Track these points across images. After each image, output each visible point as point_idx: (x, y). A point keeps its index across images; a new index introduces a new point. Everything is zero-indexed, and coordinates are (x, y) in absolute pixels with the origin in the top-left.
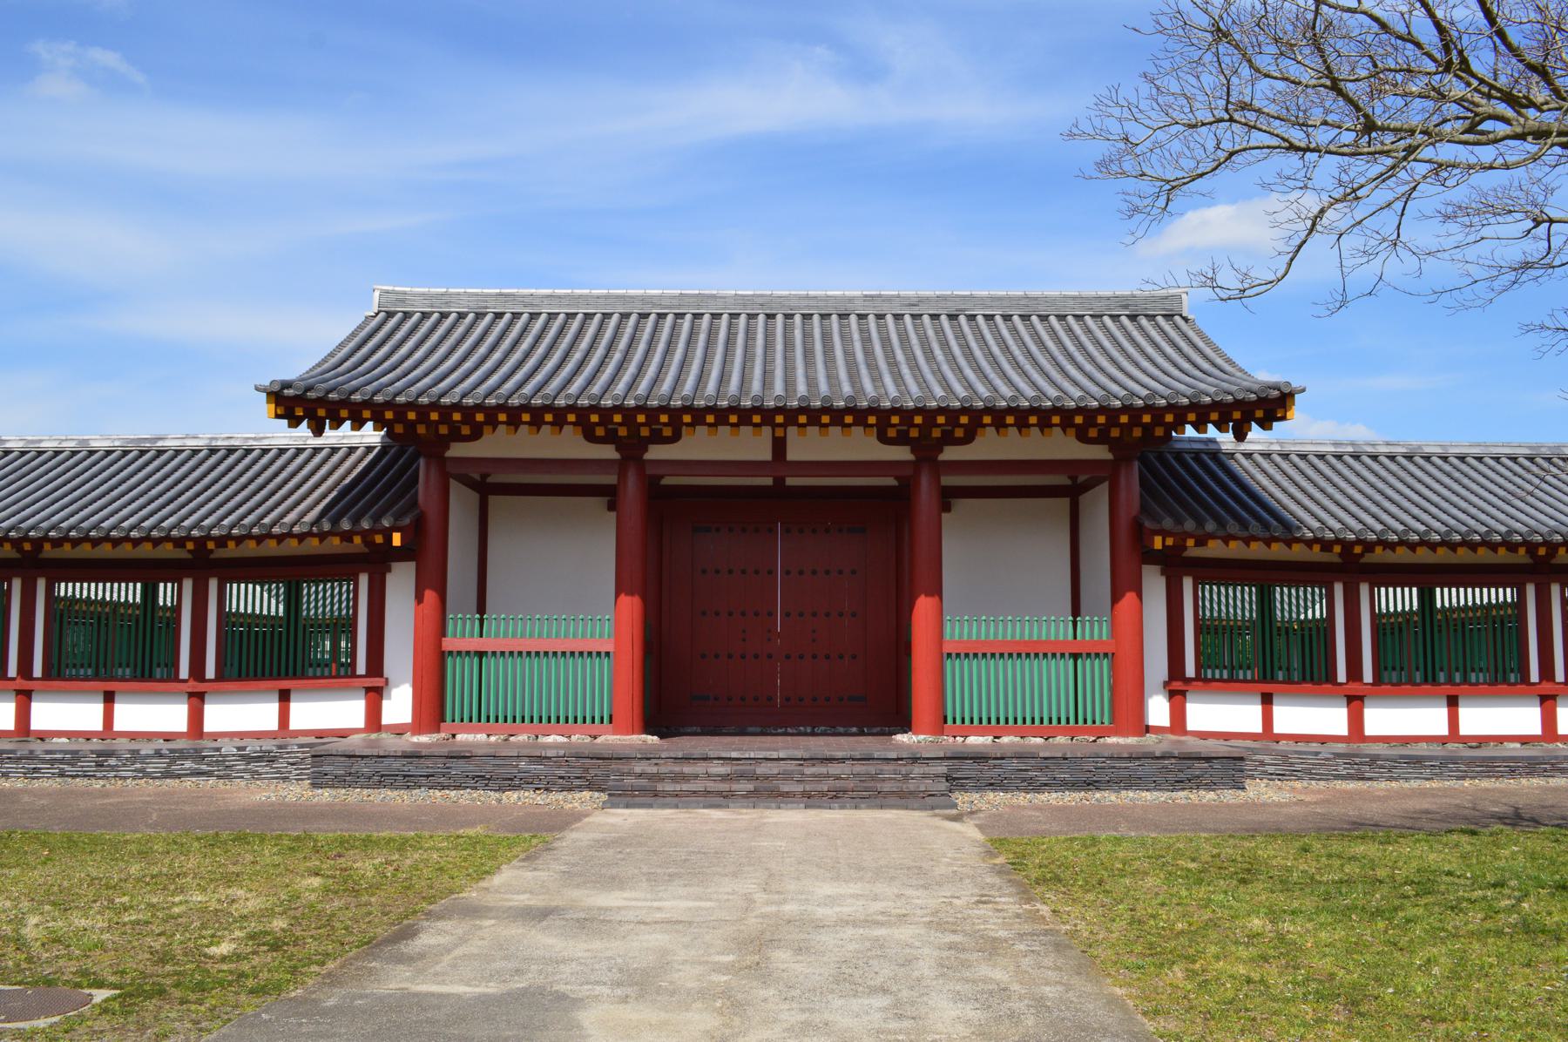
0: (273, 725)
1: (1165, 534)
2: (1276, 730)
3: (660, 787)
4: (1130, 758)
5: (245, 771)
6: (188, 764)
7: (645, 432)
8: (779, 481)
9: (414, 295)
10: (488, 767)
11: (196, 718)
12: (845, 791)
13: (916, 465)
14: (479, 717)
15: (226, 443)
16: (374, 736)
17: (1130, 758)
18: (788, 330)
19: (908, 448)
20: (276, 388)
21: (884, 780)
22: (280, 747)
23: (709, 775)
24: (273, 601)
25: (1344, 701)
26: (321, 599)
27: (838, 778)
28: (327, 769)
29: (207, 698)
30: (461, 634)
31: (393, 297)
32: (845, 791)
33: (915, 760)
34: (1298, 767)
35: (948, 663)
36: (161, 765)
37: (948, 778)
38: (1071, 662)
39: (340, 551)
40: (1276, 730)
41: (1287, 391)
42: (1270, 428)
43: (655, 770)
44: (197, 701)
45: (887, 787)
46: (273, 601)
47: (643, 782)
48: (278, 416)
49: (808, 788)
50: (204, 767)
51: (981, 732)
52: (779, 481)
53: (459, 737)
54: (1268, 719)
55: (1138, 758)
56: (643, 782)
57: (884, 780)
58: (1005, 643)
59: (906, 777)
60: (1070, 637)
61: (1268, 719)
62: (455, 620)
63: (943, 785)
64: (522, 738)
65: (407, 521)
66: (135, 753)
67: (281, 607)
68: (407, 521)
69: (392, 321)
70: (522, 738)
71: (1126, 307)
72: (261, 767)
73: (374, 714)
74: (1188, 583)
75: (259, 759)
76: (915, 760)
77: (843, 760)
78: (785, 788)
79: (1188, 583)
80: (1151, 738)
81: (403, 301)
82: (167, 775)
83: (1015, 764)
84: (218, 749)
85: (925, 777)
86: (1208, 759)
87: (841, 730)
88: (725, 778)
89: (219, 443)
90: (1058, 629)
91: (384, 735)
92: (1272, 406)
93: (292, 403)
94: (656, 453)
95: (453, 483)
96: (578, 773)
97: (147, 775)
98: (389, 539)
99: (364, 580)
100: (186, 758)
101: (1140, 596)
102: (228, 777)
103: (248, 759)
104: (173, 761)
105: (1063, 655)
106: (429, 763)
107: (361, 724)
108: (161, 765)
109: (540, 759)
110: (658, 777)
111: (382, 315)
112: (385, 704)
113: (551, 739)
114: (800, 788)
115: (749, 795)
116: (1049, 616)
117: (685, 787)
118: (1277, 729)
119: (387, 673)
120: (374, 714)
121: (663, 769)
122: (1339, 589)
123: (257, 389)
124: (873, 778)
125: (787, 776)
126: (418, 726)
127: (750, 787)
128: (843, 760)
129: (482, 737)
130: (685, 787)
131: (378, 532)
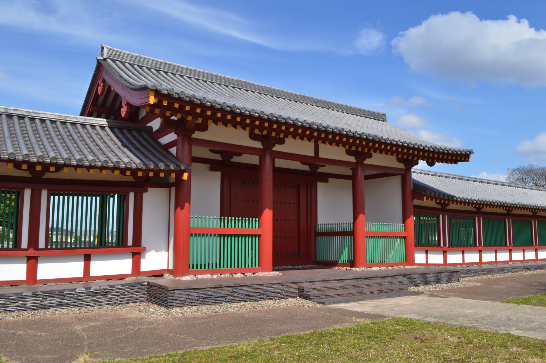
0: (81, 274)
5: (90, 301)
6: (55, 300)
9: (124, 54)
10: (250, 291)
11: (32, 272)
13: (357, 164)
19: (354, 157)
22: (111, 286)
25: (131, 255)
28: (176, 297)
29: (39, 259)
31: (114, 53)
35: (191, 238)
36: (36, 301)
38: (219, 238)
39: (119, 180)
44: (32, 263)
50: (65, 301)
54: (445, 259)
58: (209, 229)
60: (219, 227)
61: (445, 259)
62: (194, 218)
66: (19, 296)
72: (101, 299)
74: (44, 193)
75: (99, 294)
79: (44, 193)
80: (415, 267)
81: (119, 55)
82: (41, 307)
84: (74, 290)
86: (453, 272)
87: (297, 267)
90: (399, 228)
96: (285, 290)
97: (26, 308)
100: (53, 296)
101: (190, 204)
102: (80, 305)
103: (93, 294)
104: (45, 298)
105: (215, 235)
106: (225, 290)
107: (129, 272)
108: (36, 301)
112: (142, 261)
115: (356, 294)
116: (198, 216)
118: (448, 262)
119: (143, 244)
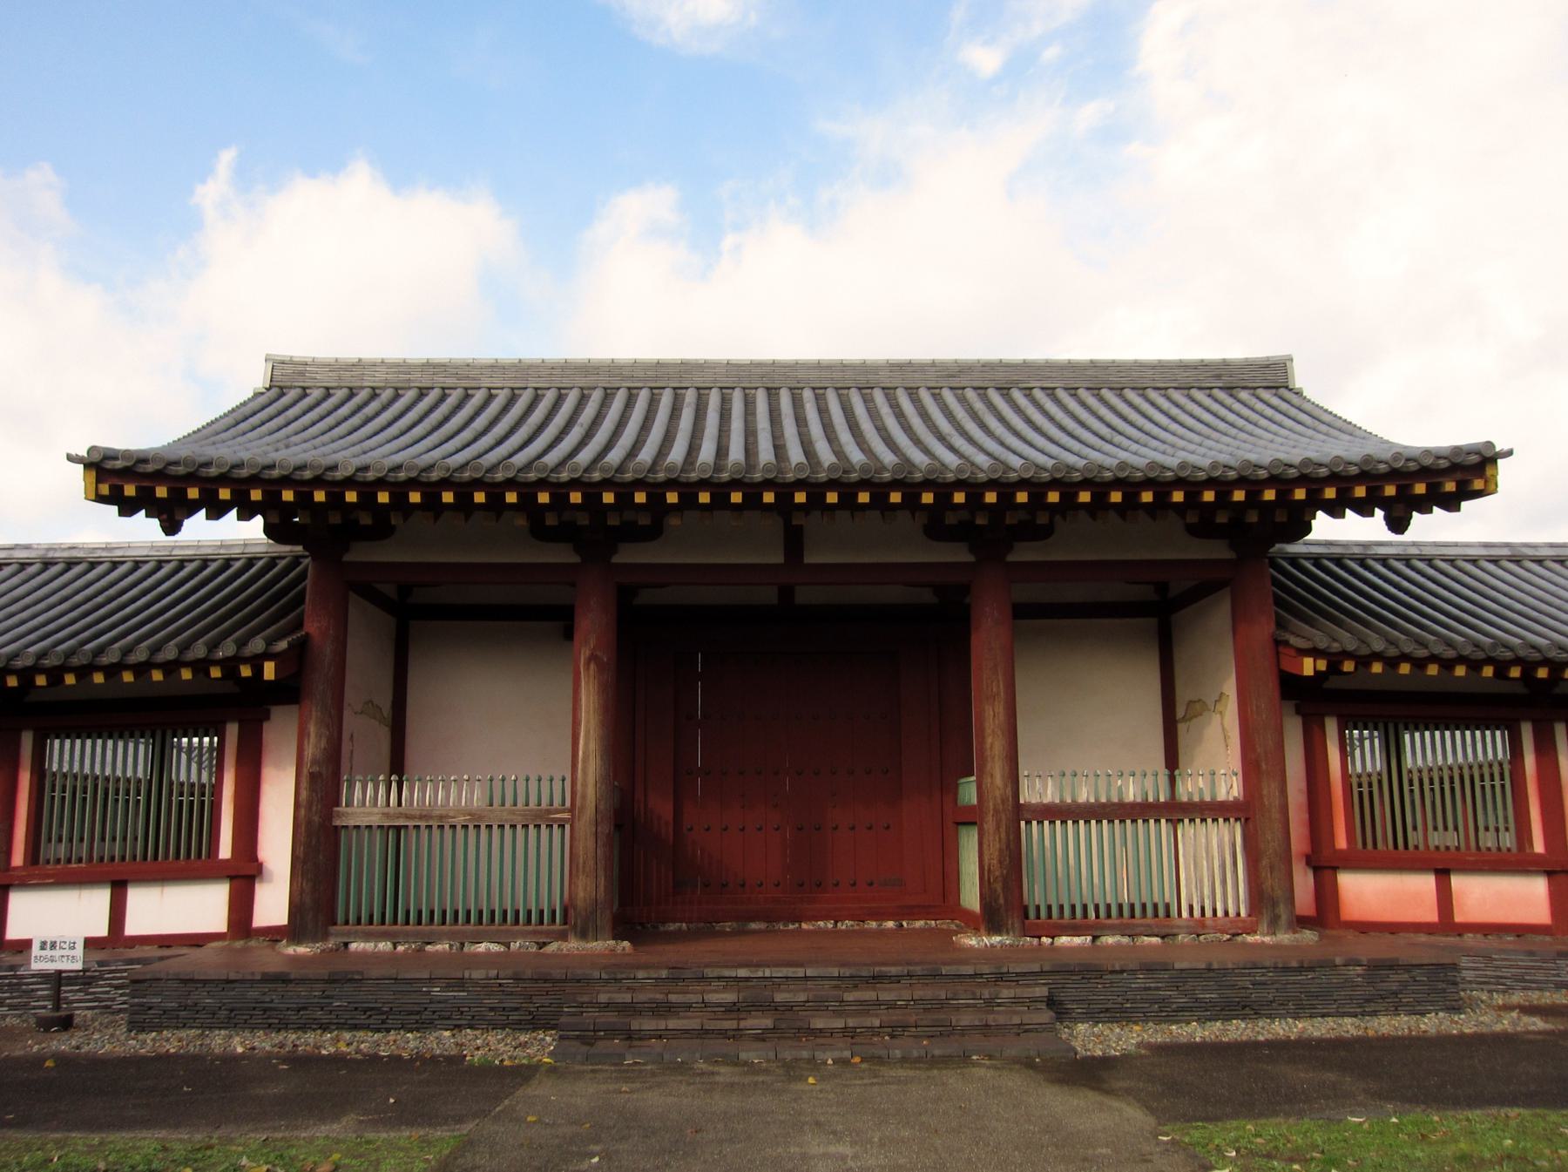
1: (1315, 653)
2: (1458, 919)
3: (635, 1025)
4: (1301, 969)
7: (613, 521)
8: (786, 592)
12: (905, 1027)
14: (372, 924)
15: (66, 554)
16: (239, 944)
17: (1301, 969)
18: (797, 403)
20: (96, 457)
21: (958, 1008)
23: (705, 1004)
24: (194, 766)
26: (191, 757)
27: (892, 1006)
30: (366, 802)
32: (905, 1027)
33: (1000, 978)
34: (1506, 972)
37: (1051, 1002)
40: (1458, 919)
41: (1488, 454)
42: (1458, 509)
43: (627, 998)
45: (966, 1019)
46: (194, 766)
47: (611, 1018)
48: (100, 499)
49: (851, 1022)
51: (1075, 931)
52: (786, 592)
53: (353, 946)
55: (1311, 969)
56: (611, 1018)
57: (958, 1008)
59: (990, 1003)
63: (1046, 1016)
64: (442, 947)
65: (283, 645)
67: (205, 775)
68: (283, 645)
69: (291, 391)
70: (442, 947)
71: (1218, 377)
73: (241, 906)
74: (1331, 726)
76: (1000, 978)
77: (897, 979)
78: (818, 1023)
81: (302, 374)
83: (1141, 980)
85: (1017, 1001)
88: (732, 1009)
89: (57, 555)
91: (253, 943)
92: (1462, 475)
93: (120, 479)
94: (629, 555)
95: (353, 596)
98: (258, 671)
99: (232, 730)
109: (461, 983)
110: (631, 1009)
111: (275, 391)
113: (482, 947)
114: (839, 1023)
117: (673, 1023)
120: (241, 906)
121: (641, 997)
122: (1527, 732)
123: (70, 458)
124: (941, 1005)
125: (819, 1005)
126: (295, 930)
127: (768, 1022)
128: (897, 979)
129: (384, 946)
130: (673, 1023)
131: (246, 660)
